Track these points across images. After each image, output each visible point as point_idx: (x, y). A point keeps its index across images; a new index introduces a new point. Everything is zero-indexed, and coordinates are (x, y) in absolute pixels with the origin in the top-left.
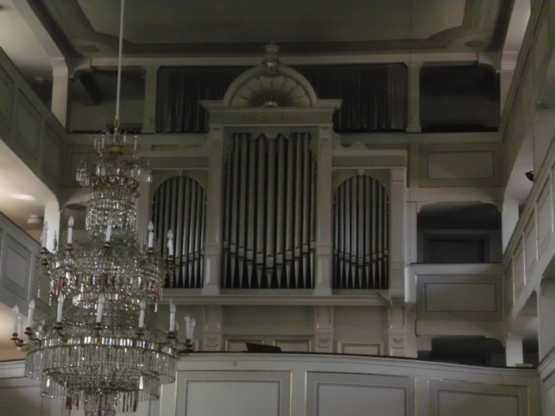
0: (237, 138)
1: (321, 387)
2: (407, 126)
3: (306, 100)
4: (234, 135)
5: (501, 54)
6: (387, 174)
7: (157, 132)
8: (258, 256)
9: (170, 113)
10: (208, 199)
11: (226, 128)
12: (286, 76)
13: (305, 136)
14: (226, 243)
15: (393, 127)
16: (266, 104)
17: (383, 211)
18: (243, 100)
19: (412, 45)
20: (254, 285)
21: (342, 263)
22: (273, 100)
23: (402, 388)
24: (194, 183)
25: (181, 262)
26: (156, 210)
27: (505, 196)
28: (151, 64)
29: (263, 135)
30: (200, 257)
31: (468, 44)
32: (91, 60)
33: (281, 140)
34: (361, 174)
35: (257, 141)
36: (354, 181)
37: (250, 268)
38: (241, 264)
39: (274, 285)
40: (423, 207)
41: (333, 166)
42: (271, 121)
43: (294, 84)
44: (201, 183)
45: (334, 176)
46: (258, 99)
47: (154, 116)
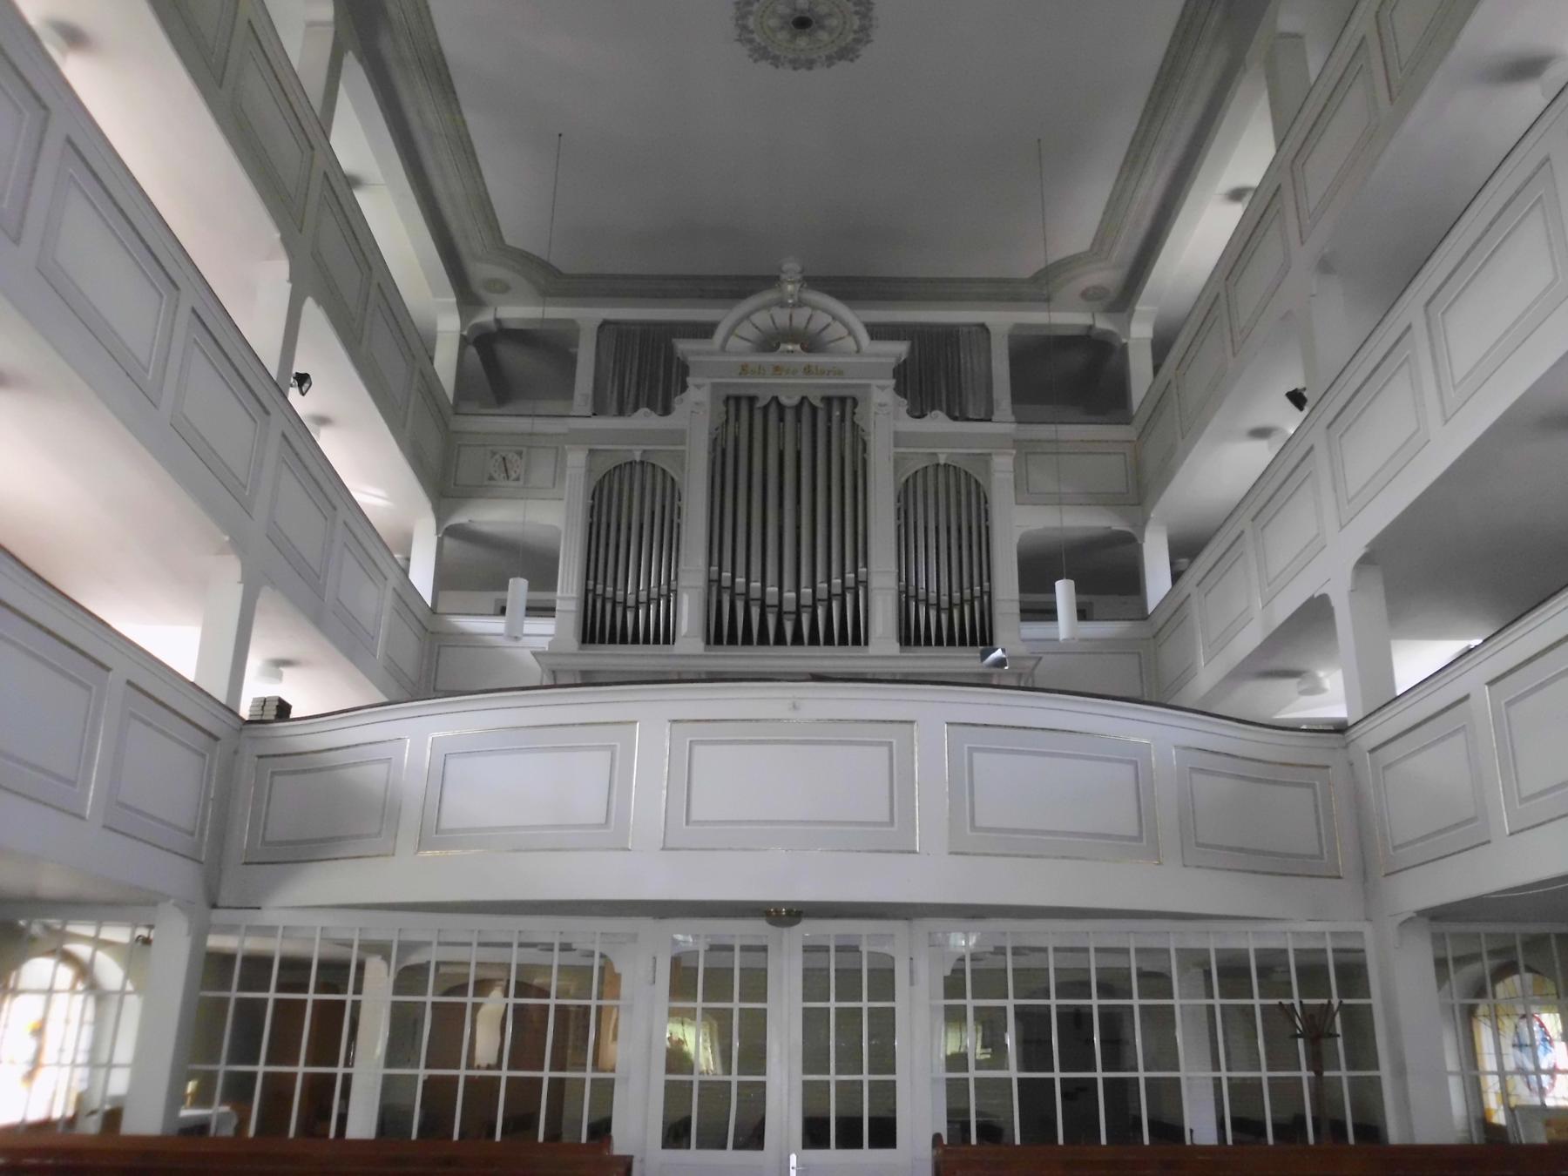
0: (737, 404)
1: (976, 755)
3: (849, 343)
6: (985, 459)
8: (769, 589)
11: (714, 385)
12: (814, 308)
13: (844, 405)
14: (715, 569)
16: (783, 347)
20: (763, 640)
22: (795, 342)
23: (1131, 762)
25: (637, 602)
29: (775, 399)
30: (670, 594)
31: (1085, 295)
33: (806, 410)
34: (942, 462)
35: (766, 409)
36: (931, 472)
37: (755, 612)
39: (797, 639)
42: (791, 378)
43: (827, 319)
45: (898, 462)
47: (590, 392)
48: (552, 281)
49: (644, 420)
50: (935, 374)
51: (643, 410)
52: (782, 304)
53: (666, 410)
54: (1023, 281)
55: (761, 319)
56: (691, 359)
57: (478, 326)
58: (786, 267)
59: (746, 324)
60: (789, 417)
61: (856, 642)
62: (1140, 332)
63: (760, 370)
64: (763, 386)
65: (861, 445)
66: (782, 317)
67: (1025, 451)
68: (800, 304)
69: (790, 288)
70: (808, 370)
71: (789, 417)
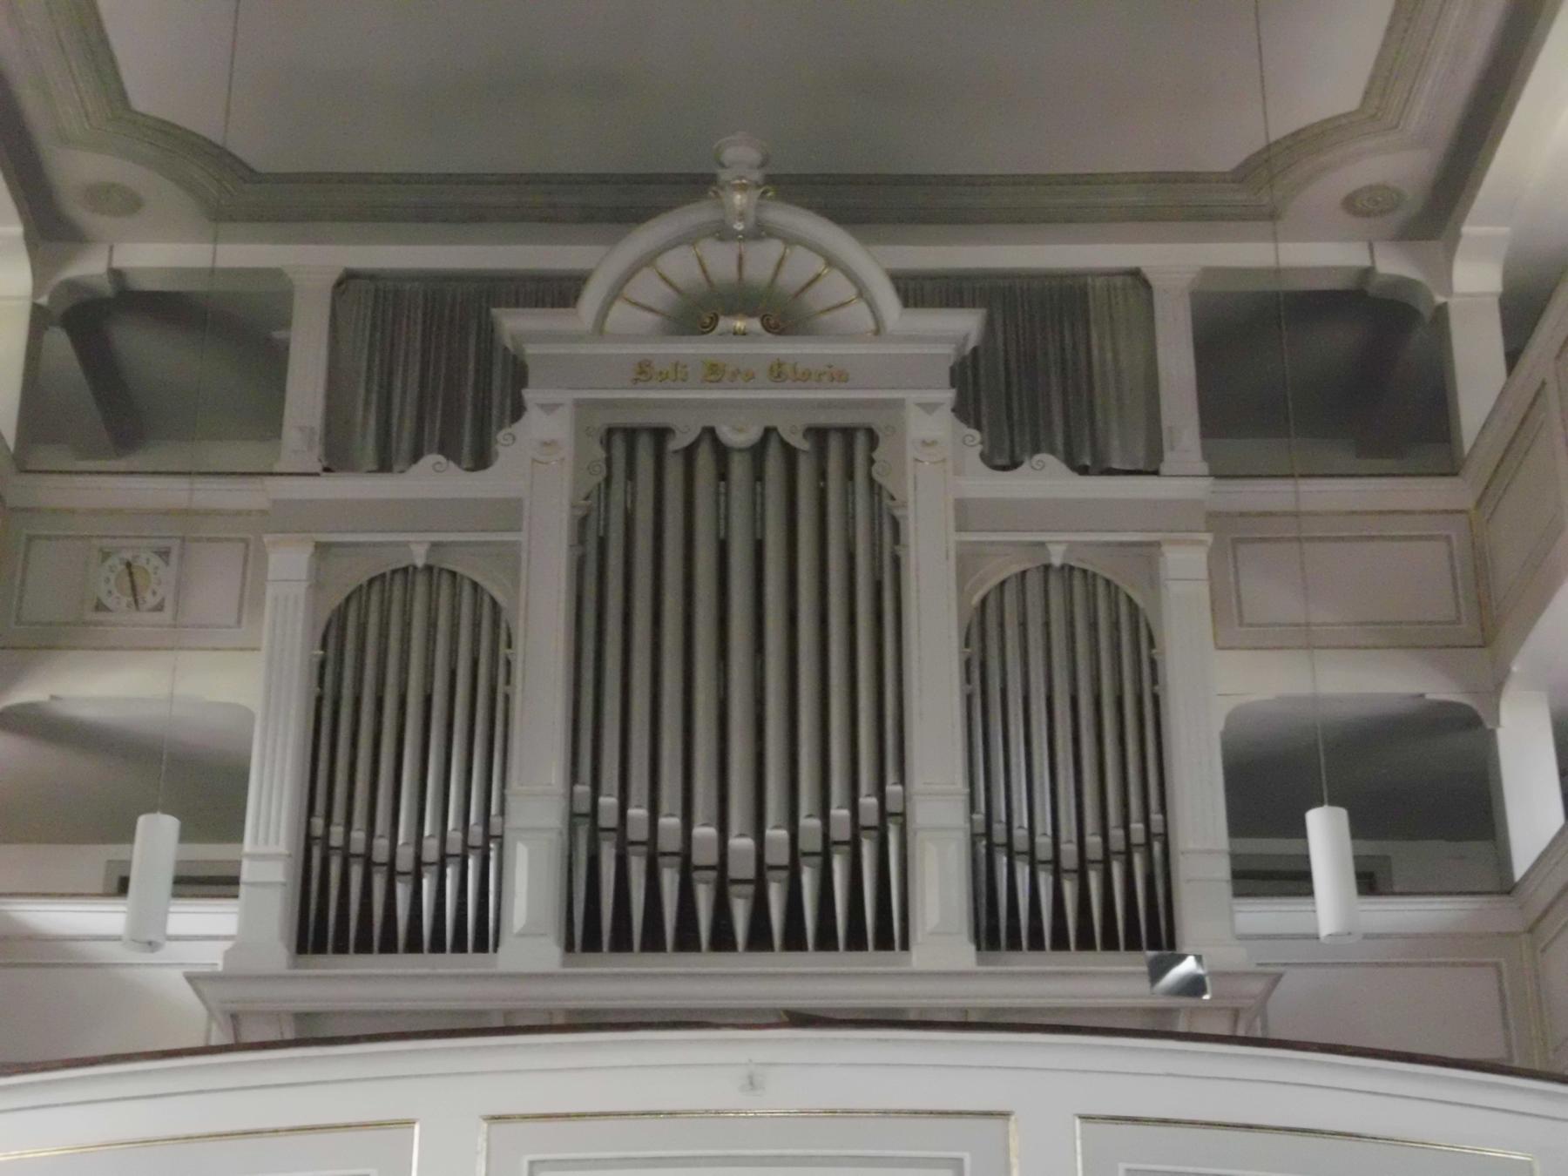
0: (630, 445)
2: (1161, 460)
4: (610, 431)
5: (1457, 237)
6: (1148, 553)
7: (327, 470)
9: (374, 397)
10: (519, 643)
12: (790, 240)
13: (847, 445)
14: (583, 789)
15: (1116, 466)
16: (724, 323)
17: (1138, 681)
18: (649, 316)
19: (1178, 200)
21: (1002, 861)
24: (467, 592)
25: (419, 862)
26: (329, 679)
27: (1515, 669)
28: (309, 263)
29: (710, 432)
30: (489, 845)
32: (111, 249)
35: (689, 453)
36: (1034, 582)
38: (637, 867)
40: (1230, 719)
41: (960, 528)
42: (740, 390)
44: (492, 588)
45: (967, 562)
46: (697, 314)
48: (234, 189)
49: (433, 479)
50: (1039, 377)
51: (431, 460)
52: (723, 233)
53: (481, 459)
54: (1221, 177)
55: (681, 266)
56: (530, 350)
57: (72, 286)
58: (729, 154)
59: (646, 275)
60: (739, 469)
61: (884, 941)
62: (1474, 279)
63: (677, 373)
64: (684, 406)
65: (888, 527)
66: (721, 261)
67: (1233, 536)
68: (760, 232)
69: (738, 199)
70: (778, 372)
71: (739, 469)
